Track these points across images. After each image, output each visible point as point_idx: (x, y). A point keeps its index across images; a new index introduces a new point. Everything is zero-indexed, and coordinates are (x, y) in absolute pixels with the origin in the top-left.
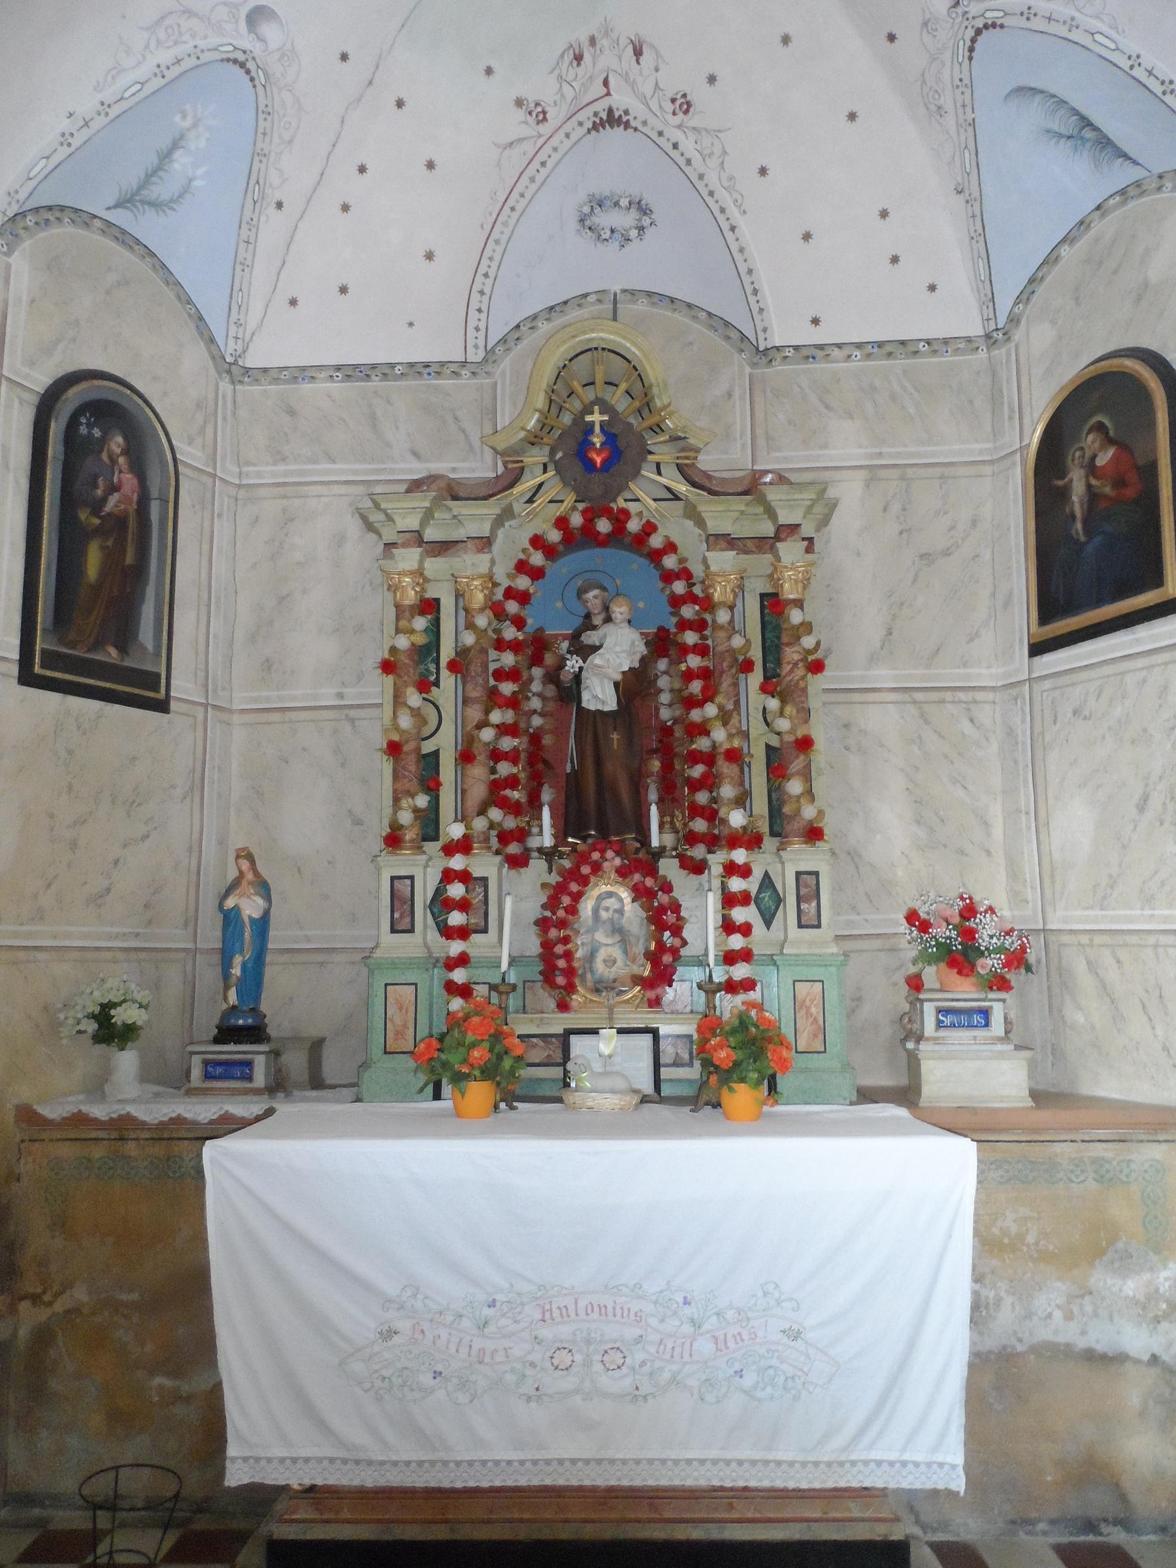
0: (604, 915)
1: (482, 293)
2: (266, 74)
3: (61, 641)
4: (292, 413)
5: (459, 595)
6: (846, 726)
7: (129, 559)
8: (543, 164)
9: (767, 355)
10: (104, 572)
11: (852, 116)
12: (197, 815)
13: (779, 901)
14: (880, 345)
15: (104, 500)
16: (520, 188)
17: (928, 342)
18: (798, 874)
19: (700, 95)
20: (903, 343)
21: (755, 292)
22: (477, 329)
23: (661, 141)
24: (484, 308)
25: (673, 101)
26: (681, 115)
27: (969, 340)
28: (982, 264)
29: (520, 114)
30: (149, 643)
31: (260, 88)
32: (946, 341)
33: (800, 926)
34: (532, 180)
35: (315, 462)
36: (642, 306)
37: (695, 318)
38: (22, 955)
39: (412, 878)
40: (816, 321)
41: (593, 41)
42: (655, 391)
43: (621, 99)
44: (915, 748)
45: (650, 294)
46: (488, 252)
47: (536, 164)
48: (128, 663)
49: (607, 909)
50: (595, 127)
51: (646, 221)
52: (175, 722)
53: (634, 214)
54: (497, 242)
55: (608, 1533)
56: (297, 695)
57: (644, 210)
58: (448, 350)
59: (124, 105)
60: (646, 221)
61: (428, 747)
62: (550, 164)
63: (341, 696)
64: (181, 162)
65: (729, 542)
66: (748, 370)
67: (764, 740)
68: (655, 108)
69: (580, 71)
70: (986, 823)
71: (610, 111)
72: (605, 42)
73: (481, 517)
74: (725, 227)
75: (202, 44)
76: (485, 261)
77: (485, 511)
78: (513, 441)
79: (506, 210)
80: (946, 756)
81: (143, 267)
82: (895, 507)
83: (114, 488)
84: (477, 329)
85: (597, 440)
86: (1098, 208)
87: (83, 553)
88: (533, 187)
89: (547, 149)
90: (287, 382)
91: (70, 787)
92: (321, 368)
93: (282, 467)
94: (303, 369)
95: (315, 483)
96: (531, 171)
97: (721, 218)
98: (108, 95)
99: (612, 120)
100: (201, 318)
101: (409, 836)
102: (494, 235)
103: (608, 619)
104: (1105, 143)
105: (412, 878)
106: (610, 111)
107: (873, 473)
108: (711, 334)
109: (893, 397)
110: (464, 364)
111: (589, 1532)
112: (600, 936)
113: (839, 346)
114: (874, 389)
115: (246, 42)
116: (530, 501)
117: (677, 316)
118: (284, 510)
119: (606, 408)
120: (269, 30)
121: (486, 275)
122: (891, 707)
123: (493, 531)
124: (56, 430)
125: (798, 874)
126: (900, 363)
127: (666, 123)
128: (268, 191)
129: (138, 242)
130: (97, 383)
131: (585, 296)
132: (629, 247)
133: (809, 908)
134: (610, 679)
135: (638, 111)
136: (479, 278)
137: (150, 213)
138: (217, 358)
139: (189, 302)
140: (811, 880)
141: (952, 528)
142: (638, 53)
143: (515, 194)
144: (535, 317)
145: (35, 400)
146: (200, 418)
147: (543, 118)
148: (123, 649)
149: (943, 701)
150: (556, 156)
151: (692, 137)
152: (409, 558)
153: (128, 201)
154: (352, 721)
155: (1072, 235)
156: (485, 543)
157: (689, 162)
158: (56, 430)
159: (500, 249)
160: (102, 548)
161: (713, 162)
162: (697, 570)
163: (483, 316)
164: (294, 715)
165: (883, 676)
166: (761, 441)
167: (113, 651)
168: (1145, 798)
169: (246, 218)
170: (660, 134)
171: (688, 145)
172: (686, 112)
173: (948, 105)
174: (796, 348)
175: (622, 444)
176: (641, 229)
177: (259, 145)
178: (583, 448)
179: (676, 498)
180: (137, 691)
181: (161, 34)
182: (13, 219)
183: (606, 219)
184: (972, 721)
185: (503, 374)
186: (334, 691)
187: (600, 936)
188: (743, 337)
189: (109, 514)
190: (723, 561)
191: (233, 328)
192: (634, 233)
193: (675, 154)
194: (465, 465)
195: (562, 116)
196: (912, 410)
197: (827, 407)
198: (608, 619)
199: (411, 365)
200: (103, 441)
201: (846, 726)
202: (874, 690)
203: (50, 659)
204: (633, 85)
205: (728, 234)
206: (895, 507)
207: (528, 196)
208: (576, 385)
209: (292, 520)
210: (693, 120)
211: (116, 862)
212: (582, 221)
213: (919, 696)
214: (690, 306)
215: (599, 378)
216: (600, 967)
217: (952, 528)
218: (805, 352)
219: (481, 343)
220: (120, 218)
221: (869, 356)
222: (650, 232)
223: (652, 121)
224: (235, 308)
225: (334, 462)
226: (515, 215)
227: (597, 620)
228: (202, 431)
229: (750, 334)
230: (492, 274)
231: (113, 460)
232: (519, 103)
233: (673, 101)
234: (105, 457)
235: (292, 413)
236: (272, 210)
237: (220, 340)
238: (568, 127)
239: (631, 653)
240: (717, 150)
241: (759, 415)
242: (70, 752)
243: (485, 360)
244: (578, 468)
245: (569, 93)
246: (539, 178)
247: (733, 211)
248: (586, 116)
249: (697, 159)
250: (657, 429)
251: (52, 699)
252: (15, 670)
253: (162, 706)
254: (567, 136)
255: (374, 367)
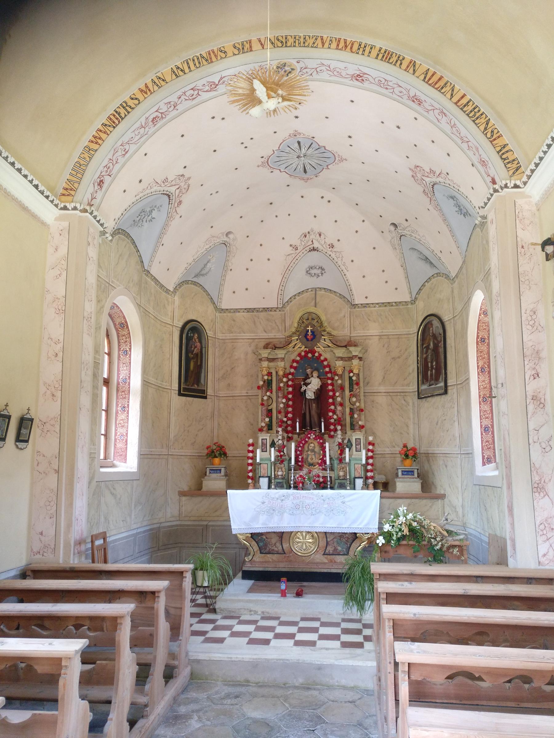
0: (310, 448)
1: (282, 290)
2: (229, 244)
3: (186, 385)
4: (234, 321)
5: (277, 372)
6: (373, 401)
7: (199, 363)
8: (297, 259)
9: (354, 306)
10: (194, 368)
11: (374, 248)
12: (213, 423)
13: (352, 445)
14: (383, 303)
15: (194, 351)
16: (291, 265)
17: (395, 303)
18: (356, 439)
19: (336, 243)
20: (389, 303)
21: (351, 290)
22: (281, 299)
23: (327, 254)
24: (282, 294)
25: (329, 245)
26: (331, 248)
27: (406, 302)
28: (408, 284)
29: (291, 248)
30: (203, 383)
31: (228, 247)
32: (400, 302)
33: (356, 451)
34: (294, 263)
35: (240, 333)
36: (323, 292)
37: (336, 295)
38: (179, 457)
39: (266, 439)
40: (366, 298)
41: (309, 233)
42: (323, 322)
43: (316, 245)
44: (390, 407)
45: (325, 289)
46: (283, 280)
47: (295, 259)
48: (199, 388)
49: (311, 446)
50: (310, 251)
51: (323, 272)
52: (209, 400)
53: (320, 270)
54: (286, 278)
55: (308, 570)
56: (237, 392)
57: (323, 269)
58: (273, 304)
59: (198, 258)
60: (323, 272)
61: (270, 408)
62: (299, 259)
63: (247, 393)
64: (209, 265)
65: (342, 359)
66: (349, 310)
67: (349, 406)
68: (325, 247)
69: (306, 238)
70: (407, 426)
71: (314, 248)
72: (312, 233)
73: (282, 354)
74: (343, 274)
75: (215, 242)
76: (282, 283)
77: (283, 352)
78: (289, 334)
79: (288, 270)
80: (398, 409)
81: (199, 289)
82: (386, 346)
83: (196, 347)
84: (281, 299)
85: (310, 333)
86: (433, 276)
87: (190, 363)
88: (294, 265)
89: (298, 256)
90: (232, 313)
91: (188, 418)
92: (241, 309)
93: (231, 335)
94: (237, 309)
95: (241, 339)
96: (294, 261)
97: (342, 272)
98: (195, 257)
99: (314, 249)
100: (212, 298)
101: (265, 429)
102: (285, 276)
103: (312, 376)
104: (431, 263)
105: (266, 439)
106: (314, 248)
107: (380, 337)
108: (340, 300)
109: (386, 317)
110: (277, 308)
111: (304, 570)
112: (309, 453)
113: (372, 304)
114: (381, 315)
115: (225, 239)
116: (294, 348)
117: (331, 295)
118: (233, 346)
119: (313, 326)
120: (231, 236)
121: (283, 286)
122: (384, 397)
123: (285, 356)
124: (184, 336)
125: (356, 439)
126: (388, 308)
127: (327, 250)
128: (229, 267)
129: (198, 283)
130: (192, 323)
131: (308, 289)
132: (319, 278)
133: (358, 447)
134: (312, 391)
135: (320, 247)
136: (281, 286)
137: (201, 277)
138: (216, 308)
139: (209, 295)
140: (359, 440)
141: (400, 351)
142: (320, 235)
143: (290, 267)
144: (295, 295)
145: (179, 329)
146: (212, 323)
147: (297, 249)
148: (198, 385)
149: (397, 395)
150: (300, 258)
151: (334, 253)
152: (265, 364)
153: (197, 275)
154: (250, 399)
155: (428, 280)
156: (283, 359)
157: (333, 259)
158: (184, 336)
159: (286, 280)
160: (194, 361)
161: (340, 259)
162: (332, 365)
163: (282, 296)
164: (235, 398)
165: (382, 389)
166: (352, 328)
167: (196, 386)
168: (438, 422)
169: (223, 274)
170: (326, 253)
171: (333, 255)
172: (332, 248)
173: (397, 248)
174: (361, 304)
175: (315, 333)
176: (322, 273)
177: (227, 258)
178: (306, 335)
179: (329, 347)
180: (201, 395)
181: (207, 243)
182: (175, 289)
183: (313, 272)
184: (405, 400)
185: (287, 311)
186: (246, 392)
187: (309, 453)
188: (348, 301)
189: (195, 353)
190: (339, 363)
191: (219, 300)
192: (320, 274)
193: (330, 257)
194: (278, 334)
195: (302, 249)
196: (391, 320)
197: (369, 320)
198: (312, 376)
199: (264, 308)
200: (193, 336)
201: (373, 401)
202: (380, 392)
203: (185, 389)
204: (319, 242)
205: (344, 276)
206: (386, 346)
207: (293, 267)
208: (304, 321)
209: (234, 348)
210: (334, 250)
211: (196, 435)
212: (307, 272)
213: (391, 394)
214: (335, 292)
215: (310, 319)
216: (309, 460)
217: (400, 351)
218: (364, 305)
219: (281, 302)
220: (195, 280)
221: (380, 306)
222: (324, 274)
223: (324, 250)
224: (220, 295)
225: (245, 333)
226: (290, 271)
227: (310, 376)
228: (213, 327)
229: (350, 300)
230: (284, 285)
231: (195, 341)
232: (291, 246)
233: (329, 245)
234: (193, 340)
235: (234, 321)
236: (229, 271)
237: (216, 303)
238: (303, 251)
239: (318, 385)
240: (341, 256)
241: (352, 321)
242: (188, 410)
243: (283, 307)
244: (305, 340)
245: (303, 244)
246: (296, 263)
247: (345, 271)
248: (308, 248)
249: (335, 258)
250: (325, 331)
251: (184, 398)
252: (177, 392)
253: (205, 398)
254: (303, 253)
255: (255, 309)
